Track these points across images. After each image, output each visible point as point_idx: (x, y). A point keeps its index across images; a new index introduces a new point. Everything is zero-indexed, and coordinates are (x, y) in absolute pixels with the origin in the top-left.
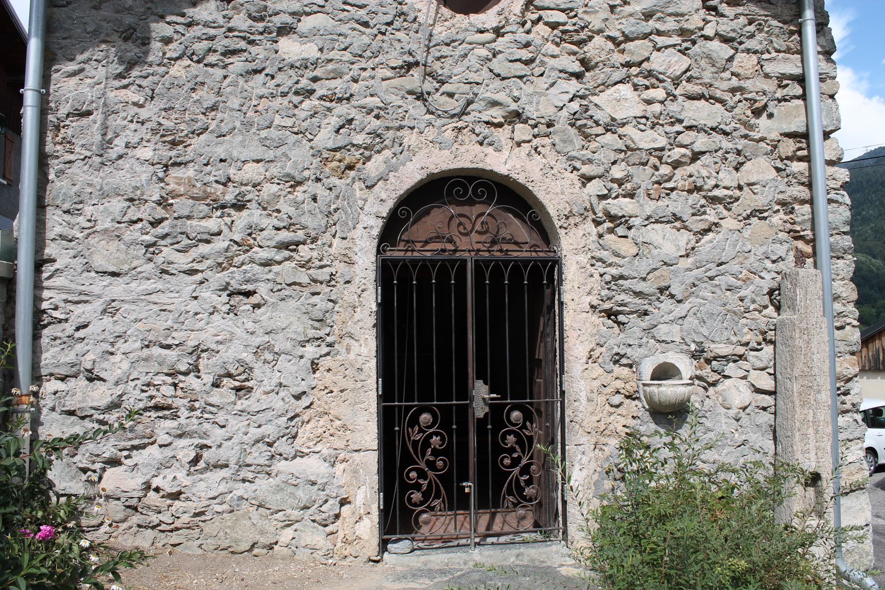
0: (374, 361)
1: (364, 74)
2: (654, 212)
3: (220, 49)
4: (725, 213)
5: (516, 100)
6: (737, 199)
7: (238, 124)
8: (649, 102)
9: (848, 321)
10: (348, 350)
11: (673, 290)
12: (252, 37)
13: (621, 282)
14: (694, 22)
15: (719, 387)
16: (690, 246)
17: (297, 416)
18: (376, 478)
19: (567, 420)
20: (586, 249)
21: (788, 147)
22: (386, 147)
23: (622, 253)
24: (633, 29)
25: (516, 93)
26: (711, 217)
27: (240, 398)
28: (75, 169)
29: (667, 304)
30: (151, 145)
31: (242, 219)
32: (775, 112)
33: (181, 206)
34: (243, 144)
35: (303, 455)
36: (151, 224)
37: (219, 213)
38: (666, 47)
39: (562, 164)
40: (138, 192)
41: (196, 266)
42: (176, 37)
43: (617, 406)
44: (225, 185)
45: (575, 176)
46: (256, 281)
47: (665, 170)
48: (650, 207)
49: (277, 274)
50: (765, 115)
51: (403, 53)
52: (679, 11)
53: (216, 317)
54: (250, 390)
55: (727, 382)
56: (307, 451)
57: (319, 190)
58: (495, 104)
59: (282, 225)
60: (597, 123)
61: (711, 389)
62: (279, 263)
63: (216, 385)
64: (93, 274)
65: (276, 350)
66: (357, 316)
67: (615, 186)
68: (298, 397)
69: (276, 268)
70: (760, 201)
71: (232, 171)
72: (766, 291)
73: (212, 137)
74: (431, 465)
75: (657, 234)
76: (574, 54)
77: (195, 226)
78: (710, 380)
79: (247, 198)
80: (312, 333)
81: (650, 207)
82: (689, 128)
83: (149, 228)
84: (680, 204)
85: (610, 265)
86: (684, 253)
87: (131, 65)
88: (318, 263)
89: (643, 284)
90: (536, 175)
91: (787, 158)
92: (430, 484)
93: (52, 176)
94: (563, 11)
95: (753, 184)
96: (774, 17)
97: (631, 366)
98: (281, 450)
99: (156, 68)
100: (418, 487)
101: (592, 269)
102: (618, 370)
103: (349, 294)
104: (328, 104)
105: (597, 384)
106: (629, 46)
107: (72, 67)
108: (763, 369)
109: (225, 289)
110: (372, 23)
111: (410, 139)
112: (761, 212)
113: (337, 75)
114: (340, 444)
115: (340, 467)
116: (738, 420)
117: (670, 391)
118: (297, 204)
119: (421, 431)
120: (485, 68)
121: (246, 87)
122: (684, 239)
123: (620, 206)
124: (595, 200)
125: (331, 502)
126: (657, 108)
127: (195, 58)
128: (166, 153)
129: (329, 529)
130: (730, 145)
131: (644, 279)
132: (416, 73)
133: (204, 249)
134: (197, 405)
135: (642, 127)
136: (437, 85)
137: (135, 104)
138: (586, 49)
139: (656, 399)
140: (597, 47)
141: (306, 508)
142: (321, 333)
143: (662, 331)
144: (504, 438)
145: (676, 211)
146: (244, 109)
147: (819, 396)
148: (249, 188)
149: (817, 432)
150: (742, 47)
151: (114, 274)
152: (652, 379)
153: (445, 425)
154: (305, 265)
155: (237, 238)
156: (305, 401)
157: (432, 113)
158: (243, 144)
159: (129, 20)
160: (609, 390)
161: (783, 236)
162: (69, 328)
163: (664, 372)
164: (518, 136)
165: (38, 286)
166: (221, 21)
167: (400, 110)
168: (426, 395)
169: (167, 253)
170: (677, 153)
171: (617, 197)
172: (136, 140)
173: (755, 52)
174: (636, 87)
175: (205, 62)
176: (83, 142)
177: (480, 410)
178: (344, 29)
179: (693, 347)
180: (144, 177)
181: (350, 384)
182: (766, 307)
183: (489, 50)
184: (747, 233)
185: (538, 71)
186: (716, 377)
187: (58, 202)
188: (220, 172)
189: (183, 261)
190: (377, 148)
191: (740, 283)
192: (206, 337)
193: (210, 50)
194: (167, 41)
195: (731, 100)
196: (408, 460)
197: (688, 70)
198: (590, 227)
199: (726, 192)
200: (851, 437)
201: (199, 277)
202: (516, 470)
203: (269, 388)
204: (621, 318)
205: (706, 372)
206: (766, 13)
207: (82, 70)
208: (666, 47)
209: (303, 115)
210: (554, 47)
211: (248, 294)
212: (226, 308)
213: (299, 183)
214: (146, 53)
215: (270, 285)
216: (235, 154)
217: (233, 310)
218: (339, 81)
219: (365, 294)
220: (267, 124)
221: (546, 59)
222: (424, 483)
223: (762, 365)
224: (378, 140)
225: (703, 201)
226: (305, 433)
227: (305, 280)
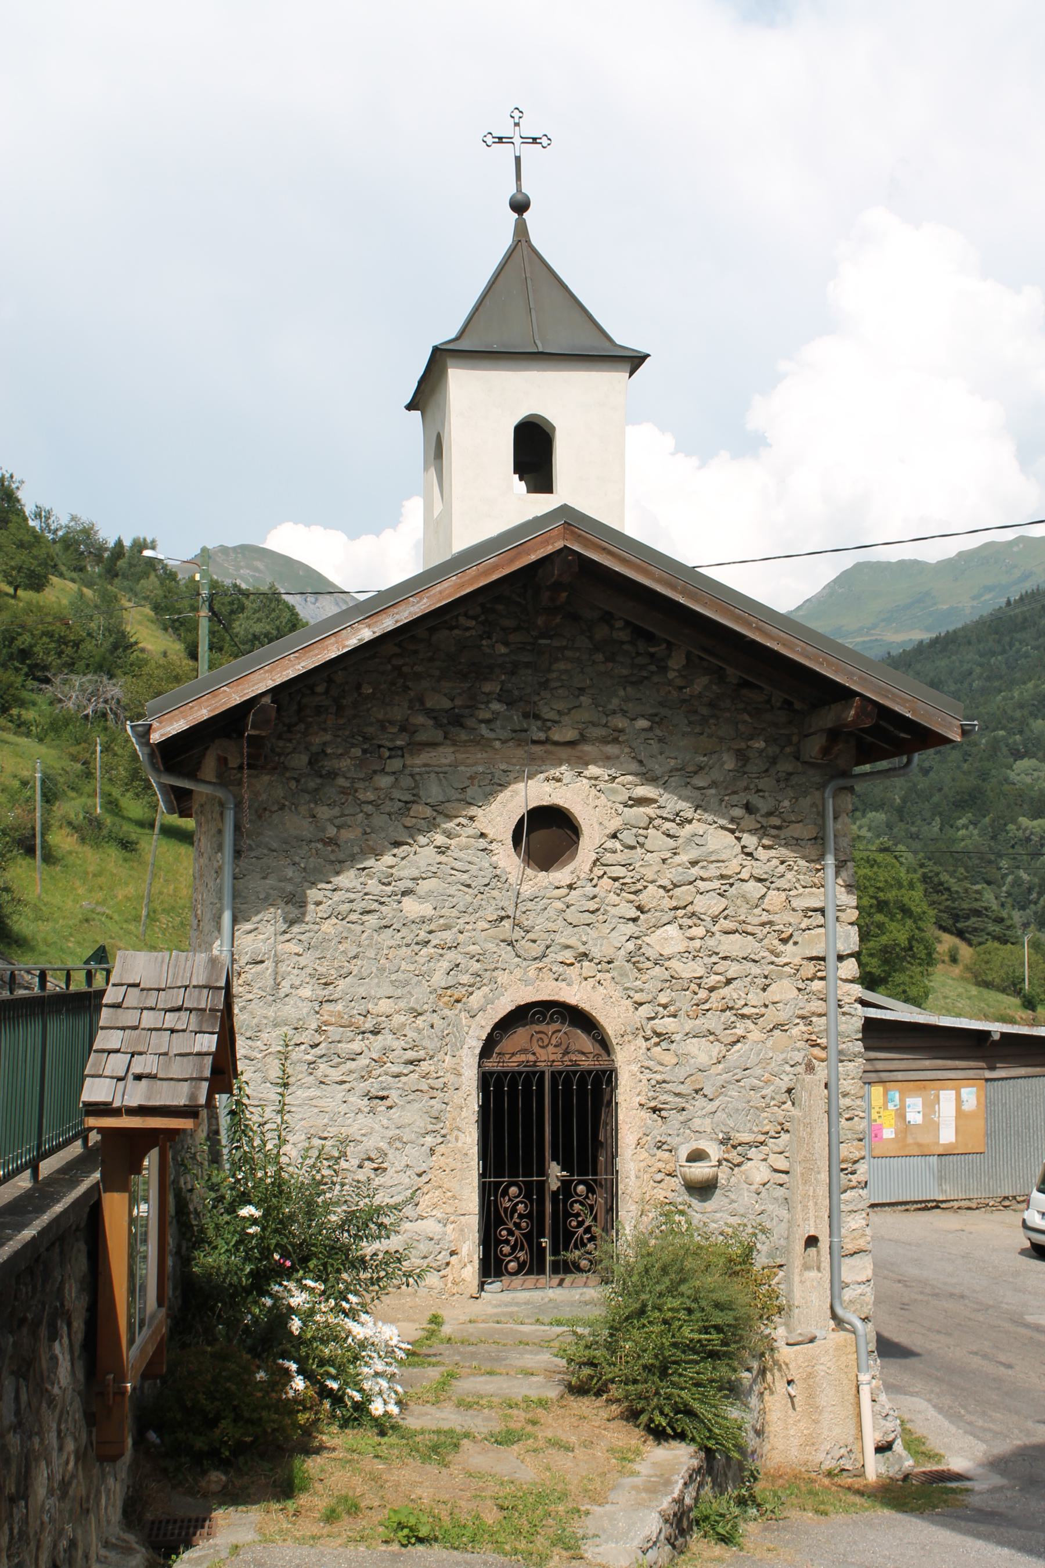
0: (476, 1148)
1: (467, 927)
2: (692, 1029)
3: (359, 910)
4: (752, 1026)
5: (584, 943)
6: (763, 1016)
7: (374, 970)
8: (691, 939)
10: (457, 1139)
11: (705, 1091)
12: (383, 900)
13: (664, 1085)
14: (732, 868)
15: (743, 1168)
16: (721, 1055)
17: (419, 1189)
18: (477, 1235)
19: (620, 1192)
20: (636, 1060)
21: (809, 969)
22: (485, 985)
23: (666, 1063)
24: (680, 878)
25: (584, 939)
26: (739, 1032)
27: (377, 1176)
28: (252, 1006)
29: (701, 1102)
30: (310, 987)
31: (378, 1042)
32: (800, 940)
33: (334, 1032)
34: (378, 985)
35: (422, 1218)
36: (311, 1046)
37: (360, 1037)
39: (617, 993)
40: (301, 1023)
41: (345, 1078)
42: (325, 900)
43: (659, 1182)
44: (365, 1016)
45: (629, 1002)
46: (390, 1089)
47: (703, 994)
48: (689, 1025)
49: (405, 1083)
50: (791, 942)
51: (497, 909)
52: (721, 859)
54: (385, 1170)
55: (750, 1163)
56: (426, 1215)
57: (435, 1019)
58: (568, 947)
59: (408, 1046)
60: (648, 959)
61: (736, 1169)
62: (406, 1075)
63: (360, 1167)
64: (268, 1084)
65: (405, 1140)
66: (464, 1114)
67: (661, 1009)
68: (420, 1175)
69: (403, 1079)
70: (782, 1016)
71: (370, 1006)
72: (784, 1089)
73: (355, 980)
74: (517, 1226)
75: (693, 1046)
76: (632, 902)
77: (344, 1048)
78: (735, 1162)
79: (382, 1026)
80: (430, 1127)
81: (689, 1025)
82: (725, 958)
83: (309, 1050)
84: (712, 1022)
85: (655, 1072)
87: (292, 923)
88: (435, 1075)
89: (682, 1086)
91: (807, 979)
92: (516, 1240)
93: (236, 1011)
95: (776, 1003)
96: (803, 858)
97: (671, 1151)
98: (407, 1214)
99: (312, 926)
100: (507, 1242)
101: (642, 1076)
102: (660, 1154)
103: (457, 1098)
104: (440, 951)
105: (643, 1164)
106: (677, 891)
108: (781, 1153)
110: (473, 885)
111: (502, 978)
112: (782, 1025)
113: (447, 927)
114: (450, 1210)
115: (450, 1227)
116: (758, 1194)
117: (700, 1171)
118: (419, 1031)
119: (510, 1200)
120: (560, 918)
121: (379, 940)
122: (717, 1049)
123: (665, 1024)
124: (644, 1022)
125: (443, 1253)
126: (697, 943)
127: (340, 917)
129: (441, 1273)
130: (759, 971)
131: (683, 1083)
132: (507, 924)
133: (351, 1065)
134: (346, 1181)
135: (684, 960)
136: (523, 934)
137: (296, 954)
138: (641, 897)
139: (688, 1177)
140: (651, 896)
141: (425, 1257)
142: (437, 1127)
143: (696, 1123)
144: (572, 1205)
145: (710, 1027)
146: (378, 957)
148: (383, 1018)
149: (816, 1204)
150: (773, 886)
152: (687, 1161)
153: (528, 1196)
154: (425, 1076)
155: (375, 1056)
156: (425, 1178)
157: (519, 957)
158: (378, 985)
159: (289, 888)
160: (653, 1169)
161: (801, 1044)
163: (696, 1156)
164: (586, 973)
166: (359, 887)
167: (495, 956)
168: (514, 1174)
169: (323, 1068)
170: (713, 979)
172: (298, 983)
173: (784, 890)
174: (681, 927)
175: (347, 920)
176: (260, 985)
177: (554, 1185)
178: (452, 890)
179: (721, 1136)
180: (305, 1011)
181: (459, 1165)
182: (784, 1103)
183: (564, 903)
184: (769, 1043)
185: (601, 918)
186: (740, 1159)
187: (243, 1031)
188: (359, 1007)
189: (335, 1075)
190: (478, 985)
191: (762, 1084)
194: (318, 904)
195: (760, 932)
196: (500, 1222)
197: (725, 909)
198: (640, 1042)
200: (855, 1209)
201: (347, 1086)
202: (581, 1230)
203: (400, 1169)
204: (664, 1113)
205: (733, 1156)
207: (256, 929)
209: (422, 960)
210: (615, 897)
211: (382, 1098)
212: (367, 1110)
213: (420, 1014)
214: (304, 914)
215: (399, 1092)
216: (373, 993)
217: (372, 1111)
218: (448, 932)
219: (469, 1098)
220: (396, 969)
221: (609, 908)
222: (512, 1239)
223: (779, 1150)
224: (478, 979)
225: (733, 1018)
226: (425, 1201)
227: (425, 1088)
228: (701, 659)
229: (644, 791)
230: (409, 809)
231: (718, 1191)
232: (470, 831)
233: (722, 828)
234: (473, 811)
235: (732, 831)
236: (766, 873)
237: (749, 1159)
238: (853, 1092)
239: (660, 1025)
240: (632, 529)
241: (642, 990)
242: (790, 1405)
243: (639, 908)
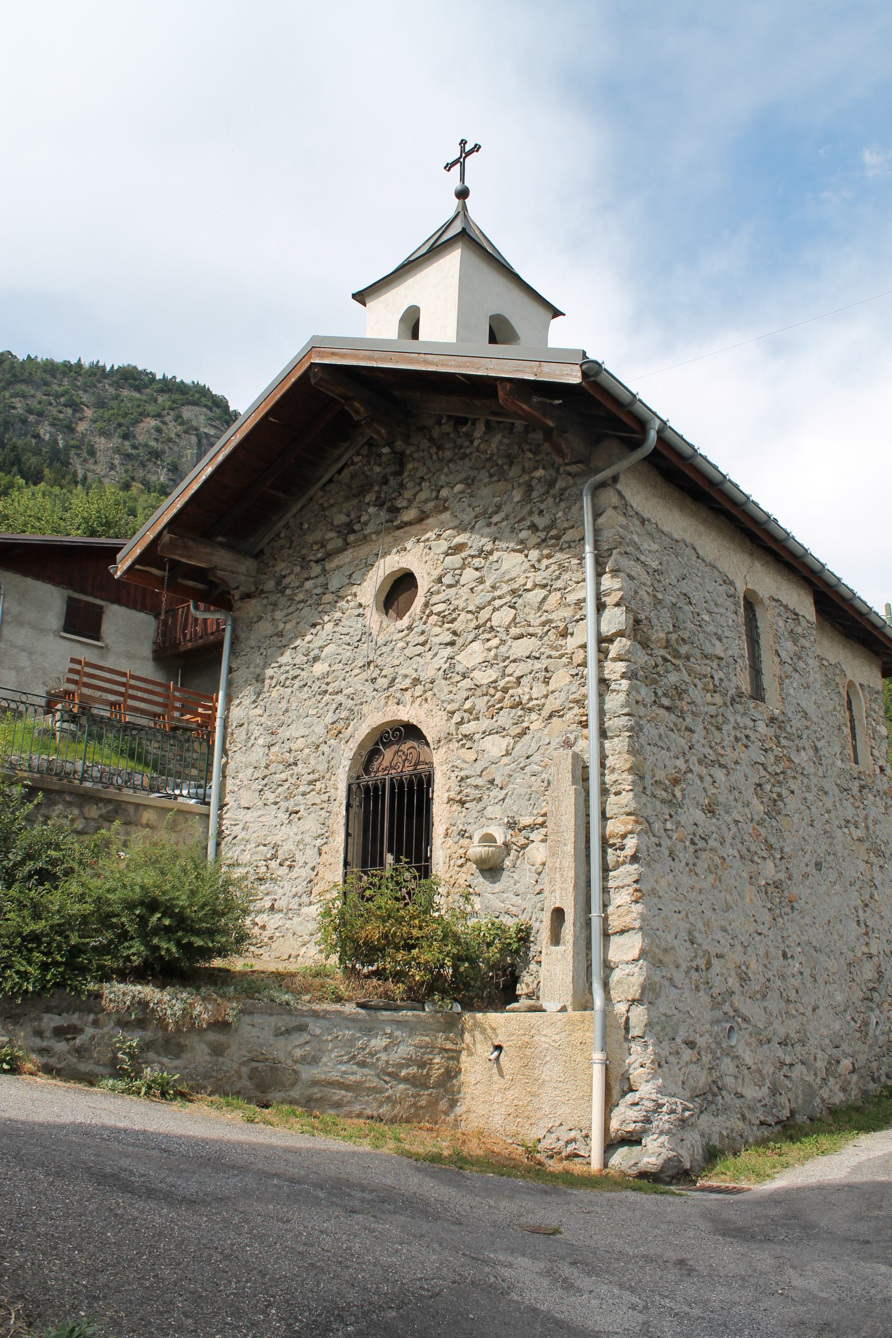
9: (623, 787)
38: (501, 607)
46: (300, 804)
52: (512, 577)
53: (283, 827)
82: (514, 661)
86: (504, 753)
90: (422, 717)
94: (444, 602)
107: (238, 701)
109: (287, 811)
123: (468, 728)
128: (269, 739)
130: (540, 666)
147: (565, 848)
151: (248, 808)
162: (230, 838)
165: (220, 817)
171: (469, 721)
191: (541, 769)
192: (277, 839)
193: (287, 679)
199: (538, 702)
200: (621, 885)
206: (567, 556)
208: (501, 607)
228: (500, 422)
229: (461, 539)
230: (320, 599)
231: (505, 873)
232: (352, 604)
233: (514, 551)
234: (355, 589)
235: (520, 551)
236: (545, 578)
237: (533, 841)
238: (617, 766)
239: (466, 729)
240: (369, 335)
241: (453, 701)
242: (495, 1070)
243: (455, 633)
